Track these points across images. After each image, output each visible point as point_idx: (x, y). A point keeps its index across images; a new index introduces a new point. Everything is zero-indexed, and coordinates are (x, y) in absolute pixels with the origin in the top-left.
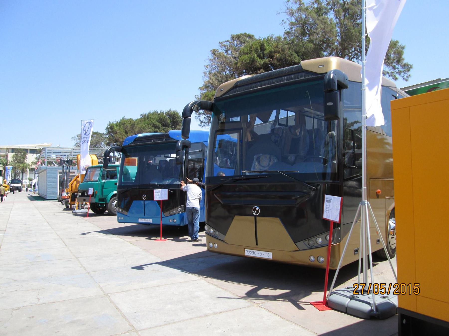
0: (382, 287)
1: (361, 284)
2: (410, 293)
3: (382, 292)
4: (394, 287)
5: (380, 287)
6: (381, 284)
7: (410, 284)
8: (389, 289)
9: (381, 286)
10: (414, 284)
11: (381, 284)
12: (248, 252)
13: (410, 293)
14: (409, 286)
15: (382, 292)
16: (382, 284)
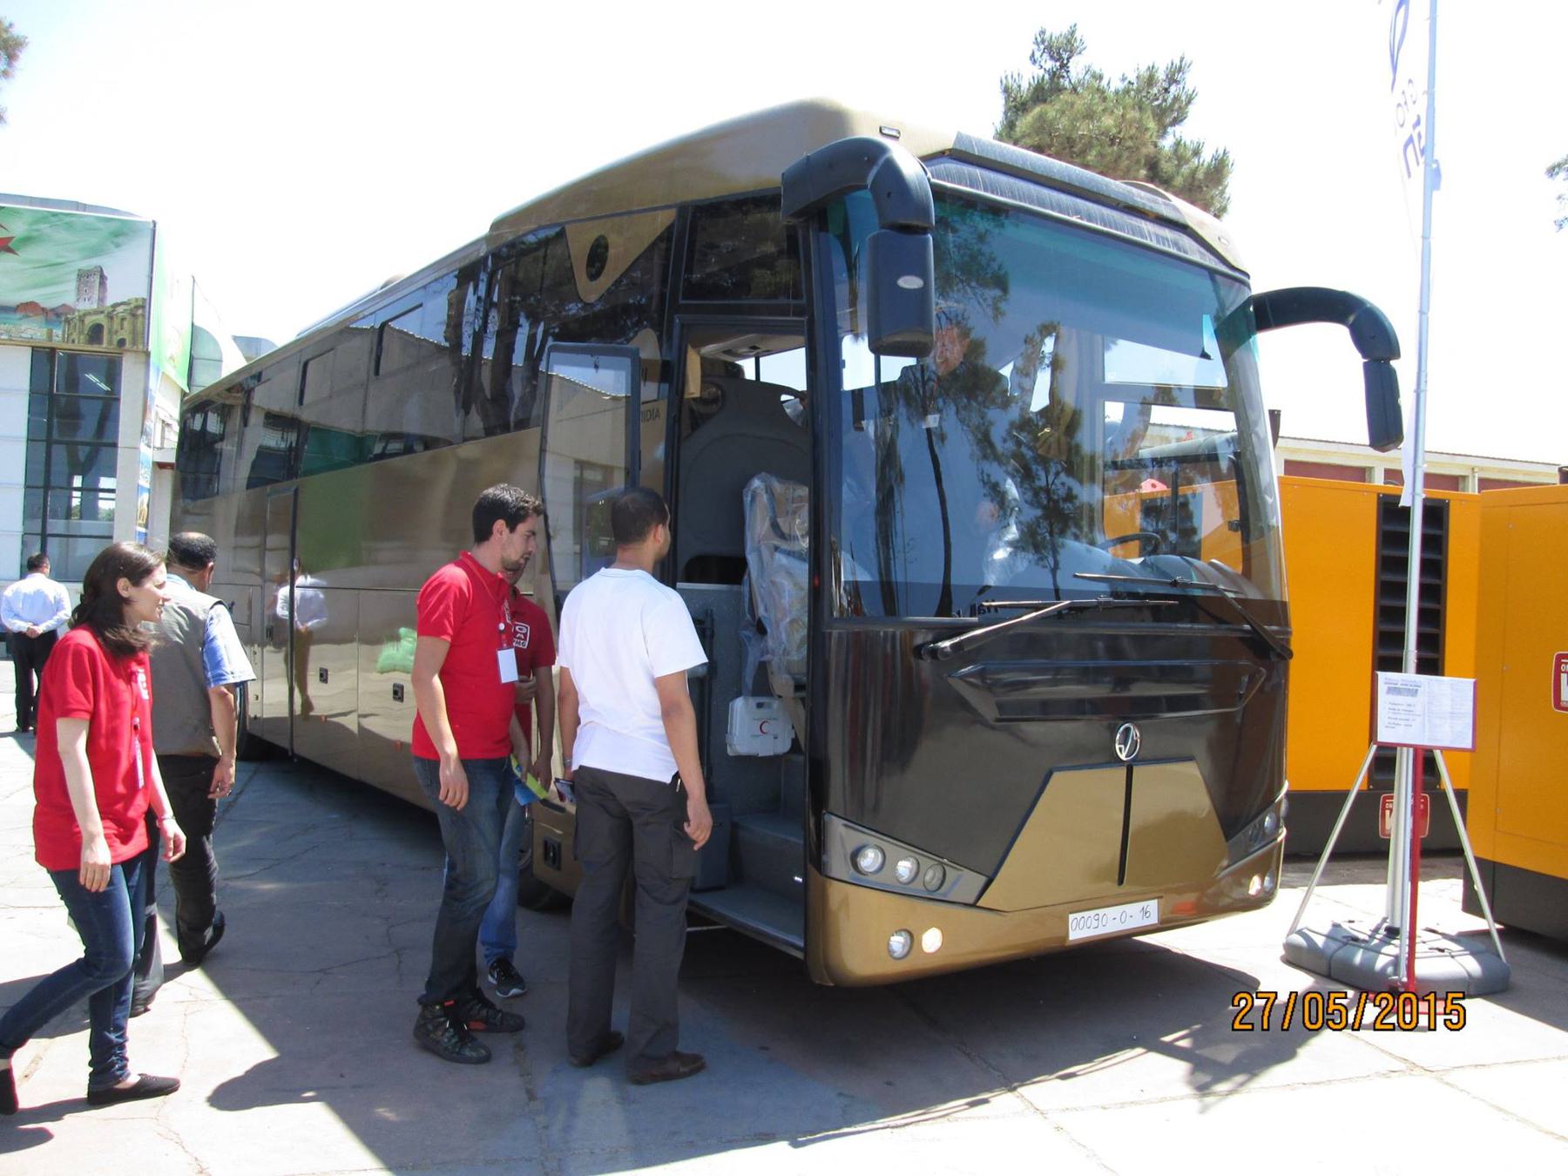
0: (1335, 1004)
1: (1259, 995)
2: (1265, 1027)
3: (1453, 1024)
4: (1377, 1003)
5: (1326, 1006)
6: (1449, 994)
7: (1433, 994)
8: (1363, 1011)
9: (1331, 1002)
10: (1447, 993)
11: (1449, 994)
12: (1078, 924)
13: (1265, 1027)
14: (1429, 1001)
15: (1453, 1024)
16: (1333, 996)
